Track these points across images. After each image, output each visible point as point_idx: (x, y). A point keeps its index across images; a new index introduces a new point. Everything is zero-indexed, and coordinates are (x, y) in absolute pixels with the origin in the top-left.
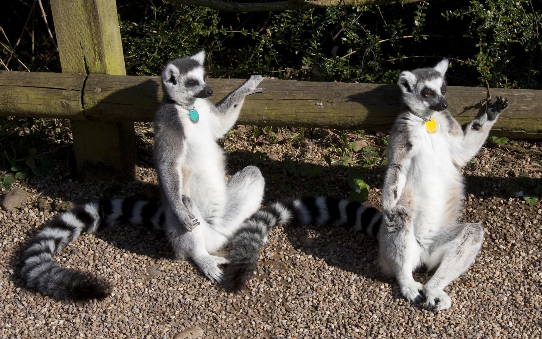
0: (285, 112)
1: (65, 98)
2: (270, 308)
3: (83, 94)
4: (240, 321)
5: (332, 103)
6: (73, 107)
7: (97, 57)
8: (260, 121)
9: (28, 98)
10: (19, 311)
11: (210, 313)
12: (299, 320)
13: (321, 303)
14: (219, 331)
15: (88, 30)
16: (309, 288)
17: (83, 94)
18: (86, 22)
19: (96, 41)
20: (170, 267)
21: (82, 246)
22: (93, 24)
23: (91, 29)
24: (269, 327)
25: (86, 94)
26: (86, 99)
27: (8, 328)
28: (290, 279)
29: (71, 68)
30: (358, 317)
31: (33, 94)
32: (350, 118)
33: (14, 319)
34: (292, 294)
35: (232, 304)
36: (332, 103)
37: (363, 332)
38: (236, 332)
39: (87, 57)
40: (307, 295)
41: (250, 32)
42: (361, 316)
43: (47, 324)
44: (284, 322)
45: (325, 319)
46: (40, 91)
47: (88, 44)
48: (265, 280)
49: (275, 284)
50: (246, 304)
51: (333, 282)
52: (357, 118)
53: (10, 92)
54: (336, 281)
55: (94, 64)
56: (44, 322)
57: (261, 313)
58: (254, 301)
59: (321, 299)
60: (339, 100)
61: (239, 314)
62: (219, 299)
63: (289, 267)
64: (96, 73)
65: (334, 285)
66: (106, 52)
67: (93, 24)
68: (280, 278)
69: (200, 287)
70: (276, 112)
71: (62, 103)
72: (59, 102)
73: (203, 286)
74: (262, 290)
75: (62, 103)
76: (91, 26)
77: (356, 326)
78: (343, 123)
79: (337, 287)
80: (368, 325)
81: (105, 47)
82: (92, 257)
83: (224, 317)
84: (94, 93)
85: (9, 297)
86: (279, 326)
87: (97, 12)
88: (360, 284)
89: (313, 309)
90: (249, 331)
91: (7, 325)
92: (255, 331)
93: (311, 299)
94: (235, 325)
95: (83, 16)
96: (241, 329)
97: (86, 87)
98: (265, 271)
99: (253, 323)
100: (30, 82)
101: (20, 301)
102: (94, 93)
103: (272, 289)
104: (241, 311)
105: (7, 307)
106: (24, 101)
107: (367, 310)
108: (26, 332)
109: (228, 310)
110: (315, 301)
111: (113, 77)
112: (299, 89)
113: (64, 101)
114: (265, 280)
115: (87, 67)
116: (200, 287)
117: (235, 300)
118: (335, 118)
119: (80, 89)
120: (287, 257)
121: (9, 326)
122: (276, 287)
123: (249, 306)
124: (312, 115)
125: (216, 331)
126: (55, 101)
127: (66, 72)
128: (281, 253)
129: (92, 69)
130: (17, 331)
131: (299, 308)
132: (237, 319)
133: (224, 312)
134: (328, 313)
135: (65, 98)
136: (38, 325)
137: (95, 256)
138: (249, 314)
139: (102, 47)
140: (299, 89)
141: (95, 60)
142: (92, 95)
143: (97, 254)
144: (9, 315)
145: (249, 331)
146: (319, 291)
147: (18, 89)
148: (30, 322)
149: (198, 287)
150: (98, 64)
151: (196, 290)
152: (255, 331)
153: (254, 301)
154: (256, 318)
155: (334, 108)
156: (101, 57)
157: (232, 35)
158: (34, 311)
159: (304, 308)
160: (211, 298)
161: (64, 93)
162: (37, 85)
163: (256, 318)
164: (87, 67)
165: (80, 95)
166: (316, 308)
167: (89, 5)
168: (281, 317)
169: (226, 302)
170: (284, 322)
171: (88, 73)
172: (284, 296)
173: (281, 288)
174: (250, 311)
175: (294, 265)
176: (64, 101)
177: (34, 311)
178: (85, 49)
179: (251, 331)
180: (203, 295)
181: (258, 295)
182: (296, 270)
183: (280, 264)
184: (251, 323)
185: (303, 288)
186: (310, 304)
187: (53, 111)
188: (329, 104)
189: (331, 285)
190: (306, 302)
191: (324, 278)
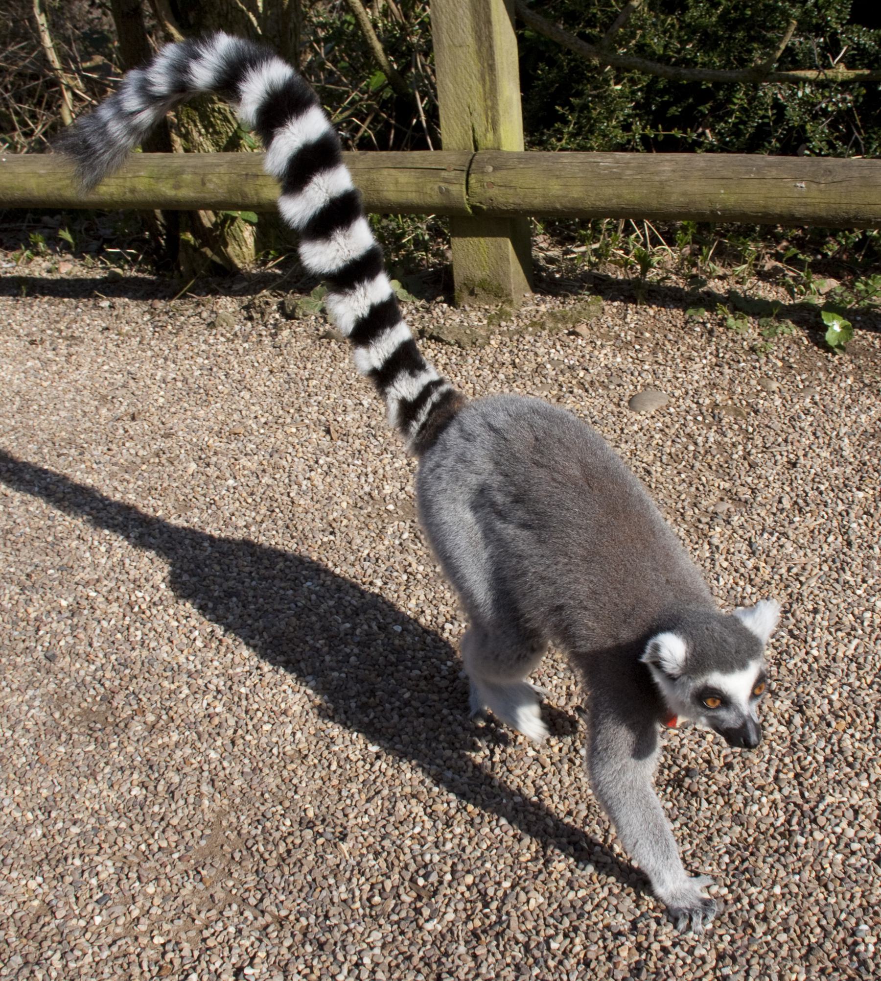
0: (750, 197)
1: (445, 181)
2: (726, 462)
3: (468, 175)
4: (683, 476)
5: (819, 183)
6: (454, 193)
7: (490, 126)
8: (712, 212)
9: (397, 183)
10: (372, 446)
11: (638, 463)
12: (771, 479)
13: (802, 458)
14: (653, 486)
15: (480, 86)
16: (780, 440)
17: (468, 175)
18: (478, 75)
19: (489, 103)
20: (578, 406)
21: (458, 378)
22: (487, 78)
23: (484, 86)
24: (727, 485)
25: (473, 176)
26: (472, 181)
27: (358, 466)
28: (751, 429)
29: (454, 144)
30: (858, 478)
31: (404, 178)
32: (844, 206)
33: (366, 455)
34: (756, 447)
35: (670, 454)
36: (819, 183)
37: (869, 496)
38: (678, 488)
39: (476, 126)
40: (779, 449)
41: (685, 132)
42: (862, 477)
43: (409, 465)
44: (749, 480)
45: (810, 478)
46: (413, 173)
47: (478, 106)
48: (715, 428)
49: (730, 434)
50: (691, 455)
51: (814, 434)
52: (854, 206)
53: (374, 175)
54: (819, 434)
55: (485, 135)
56: (405, 462)
57: (714, 468)
58: (702, 452)
59: (801, 453)
60: (830, 179)
61: (681, 467)
62: (650, 448)
63: (749, 414)
64: (487, 149)
65: (818, 438)
66: (502, 119)
67: (487, 78)
68: (736, 427)
69: (622, 432)
70: (736, 196)
71: (440, 188)
72: (436, 187)
73: (626, 431)
74: (712, 440)
75: (440, 188)
76: (484, 80)
77: (859, 489)
78: (833, 213)
79: (821, 441)
80: (874, 489)
81: (501, 112)
82: (471, 391)
83: (660, 470)
84: (483, 173)
85: (360, 431)
86: (743, 485)
87: (493, 59)
88: (854, 439)
89: (789, 466)
90: (697, 489)
91: (356, 462)
92: (707, 489)
93: (785, 454)
94: (676, 479)
95: (474, 66)
96: (685, 485)
97: (473, 166)
98: (714, 417)
99: (704, 479)
100: (400, 163)
101: (375, 436)
102: (483, 173)
103: (726, 439)
104: (684, 463)
105: (357, 442)
106: (392, 187)
107: (871, 470)
108: (381, 471)
109: (664, 461)
110: (791, 456)
111: (508, 153)
112: (770, 165)
113: (443, 186)
114: (715, 428)
115: (475, 141)
116: (622, 432)
117: (673, 450)
118: (822, 206)
119: (465, 168)
120: (744, 403)
121: (359, 462)
122: (731, 437)
123: (695, 458)
124: (789, 201)
125: (650, 486)
126: (431, 185)
127: (448, 150)
128: (735, 397)
129: (482, 144)
130: (369, 469)
131: (769, 464)
132: (679, 473)
133: (659, 464)
134: (813, 471)
135: (445, 181)
136: (396, 465)
137: (474, 389)
138: (696, 468)
139: (497, 111)
140: (770, 165)
141: (487, 130)
142: (480, 177)
143: (478, 388)
144: (359, 452)
145: (697, 489)
146: (796, 443)
147: (385, 172)
148: (386, 461)
149: (619, 432)
150: (490, 136)
151: (616, 435)
152: (707, 489)
153: (702, 452)
154: (707, 474)
155: (821, 191)
156: (494, 125)
157: (661, 138)
158: (393, 448)
159: (775, 463)
160: (639, 446)
161: (444, 174)
162: (409, 165)
163: (707, 474)
164: (475, 141)
165: (464, 175)
166: (794, 465)
167: (484, 50)
168: (743, 473)
169: (660, 451)
170: (749, 480)
171: (476, 149)
172: (745, 449)
173: (740, 438)
174: (697, 465)
175: (756, 412)
176: (443, 186)
177: (393, 448)
178: (475, 114)
179: (701, 488)
180: (626, 442)
181: (707, 445)
182: (759, 417)
183: (735, 410)
184: (700, 479)
185: (772, 439)
186: (785, 459)
187: (429, 200)
188: (814, 185)
189: (812, 438)
190: (778, 457)
191: (801, 429)
